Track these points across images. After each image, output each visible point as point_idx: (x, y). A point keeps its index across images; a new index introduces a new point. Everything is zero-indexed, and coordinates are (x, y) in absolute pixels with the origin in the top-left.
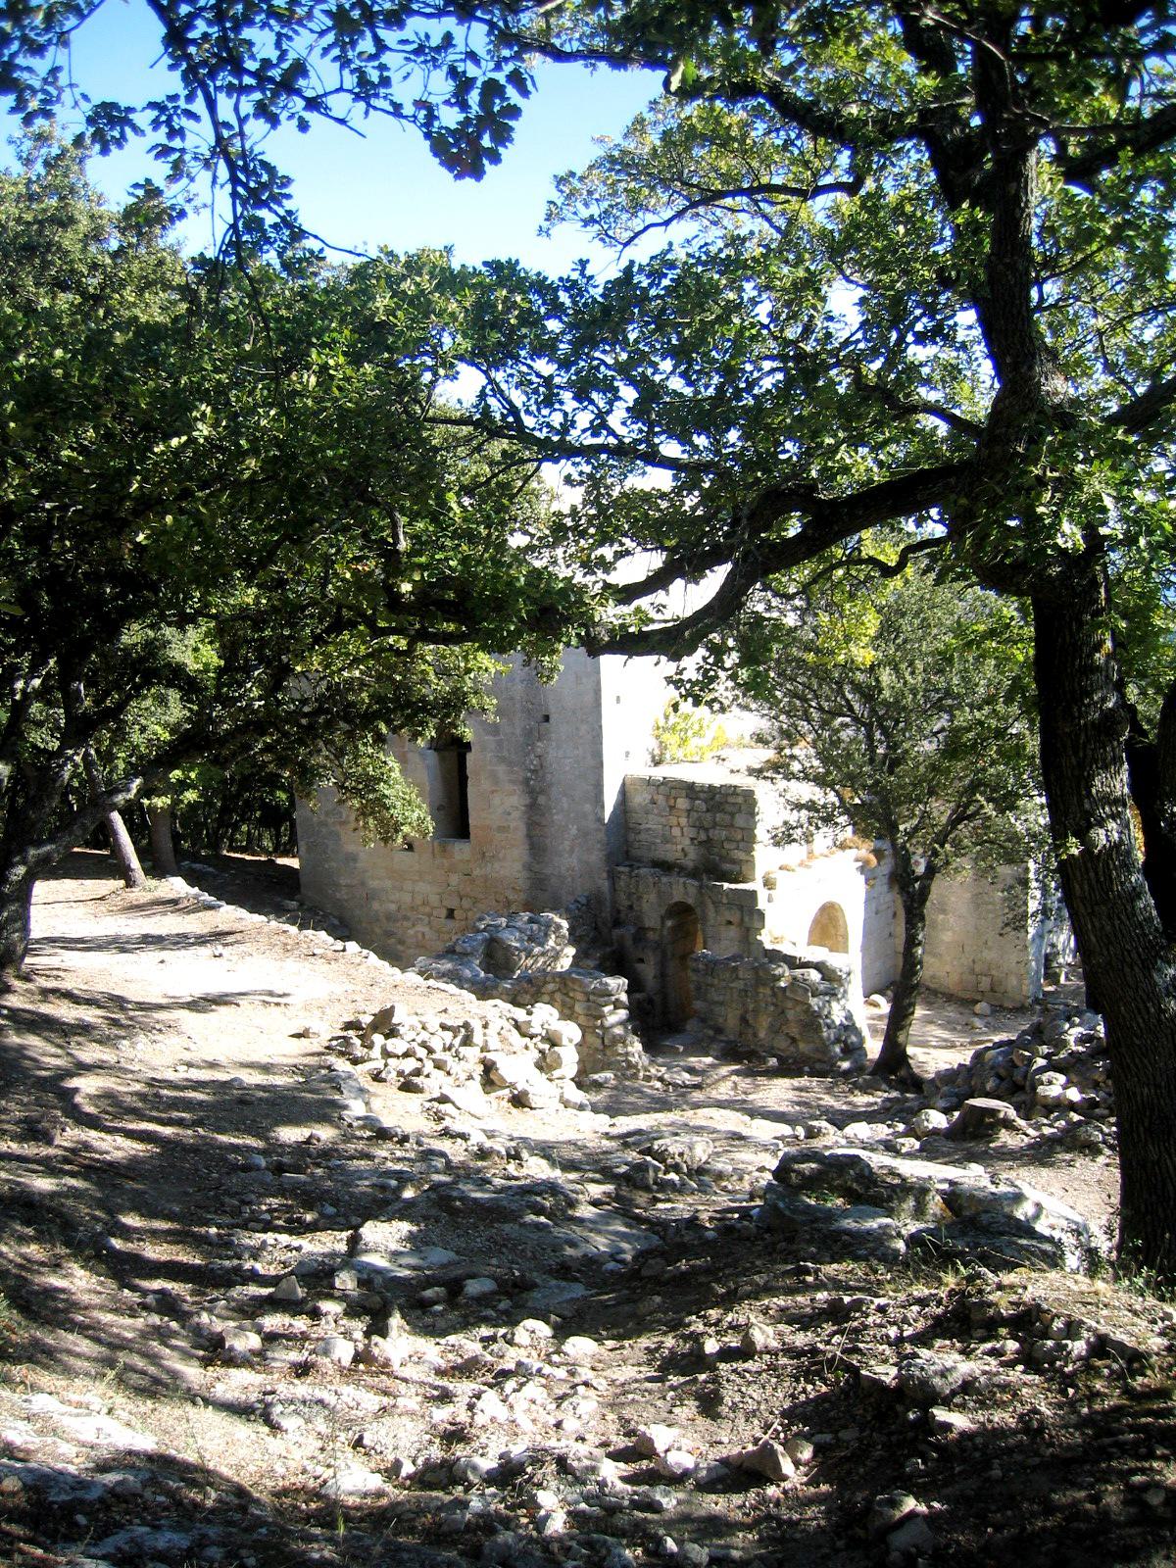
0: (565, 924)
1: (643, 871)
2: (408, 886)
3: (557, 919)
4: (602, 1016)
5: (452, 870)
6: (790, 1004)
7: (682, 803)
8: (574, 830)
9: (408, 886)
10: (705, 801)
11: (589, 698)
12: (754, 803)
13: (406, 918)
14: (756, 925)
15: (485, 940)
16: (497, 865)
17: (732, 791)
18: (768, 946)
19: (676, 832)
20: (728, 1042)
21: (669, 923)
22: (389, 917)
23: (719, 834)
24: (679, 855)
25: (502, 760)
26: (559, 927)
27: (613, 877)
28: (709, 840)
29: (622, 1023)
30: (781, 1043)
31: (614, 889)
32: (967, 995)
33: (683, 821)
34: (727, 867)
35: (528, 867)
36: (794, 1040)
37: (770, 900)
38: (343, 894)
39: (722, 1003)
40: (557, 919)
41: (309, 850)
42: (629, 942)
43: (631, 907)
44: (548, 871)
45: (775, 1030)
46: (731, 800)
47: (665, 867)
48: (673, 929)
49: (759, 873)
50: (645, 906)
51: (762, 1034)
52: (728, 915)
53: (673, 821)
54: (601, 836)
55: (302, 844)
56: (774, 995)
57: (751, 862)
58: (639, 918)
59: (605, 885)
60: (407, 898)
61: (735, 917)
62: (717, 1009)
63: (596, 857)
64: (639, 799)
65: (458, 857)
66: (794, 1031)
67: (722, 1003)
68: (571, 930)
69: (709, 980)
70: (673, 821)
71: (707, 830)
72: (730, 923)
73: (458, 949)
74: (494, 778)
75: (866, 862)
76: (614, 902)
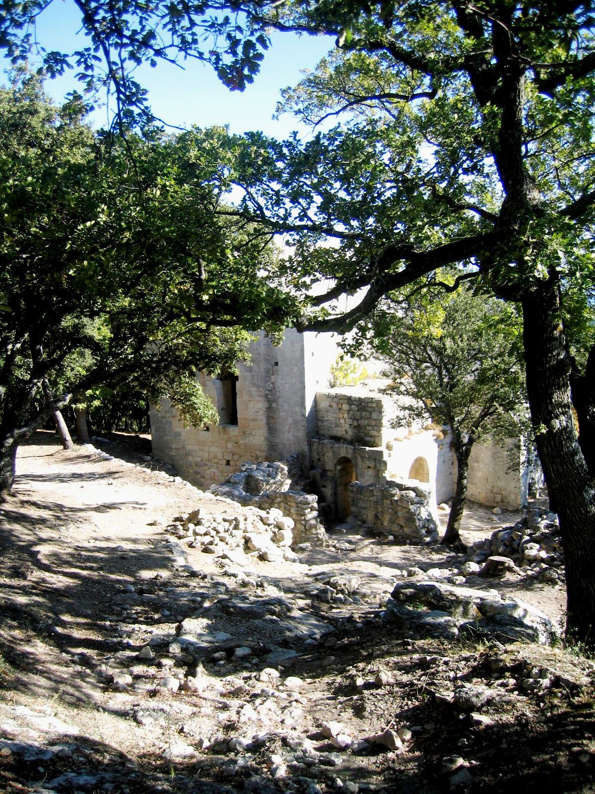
0: (286, 468)
1: (325, 441)
2: (206, 449)
3: (282, 465)
4: (304, 515)
5: (228, 440)
6: (399, 509)
7: (345, 407)
8: (290, 421)
9: (206, 449)
10: (357, 406)
11: (298, 353)
12: (381, 407)
13: (205, 465)
14: (383, 468)
15: (245, 476)
16: (251, 438)
17: (371, 400)
18: (389, 479)
19: (342, 421)
20: (368, 528)
21: (339, 468)
22: (197, 464)
23: (364, 422)
24: (344, 433)
25: (254, 385)
26: (283, 469)
27: (310, 444)
28: (359, 426)
29: (315, 518)
30: (395, 528)
31: (310, 450)
32: (487, 504)
33: (346, 416)
34: (368, 439)
35: (267, 439)
36: (402, 527)
37: (389, 456)
38: (173, 453)
39: (365, 508)
40: (282, 465)
41: (156, 430)
42: (318, 477)
43: (319, 459)
44: (277, 441)
45: (392, 522)
46: (370, 405)
47: (336, 439)
48: (340, 470)
49: (384, 442)
50: (327, 459)
51: (386, 524)
52: (368, 463)
53: (341, 416)
54: (304, 423)
55: (153, 427)
56: (392, 504)
57: (380, 437)
58: (323, 465)
59: (306, 448)
60: (206, 455)
61: (372, 464)
62: (363, 511)
63: (302, 434)
64: (323, 405)
65: (232, 434)
66: (402, 522)
67: (365, 508)
68: (289, 471)
69: (359, 496)
70: (341, 416)
71: (357, 420)
72: (369, 467)
73: (232, 481)
74: (250, 394)
75: (438, 437)
76: (311, 457)
